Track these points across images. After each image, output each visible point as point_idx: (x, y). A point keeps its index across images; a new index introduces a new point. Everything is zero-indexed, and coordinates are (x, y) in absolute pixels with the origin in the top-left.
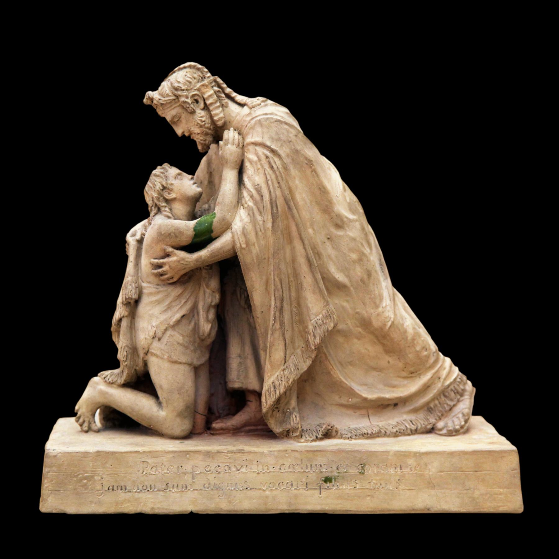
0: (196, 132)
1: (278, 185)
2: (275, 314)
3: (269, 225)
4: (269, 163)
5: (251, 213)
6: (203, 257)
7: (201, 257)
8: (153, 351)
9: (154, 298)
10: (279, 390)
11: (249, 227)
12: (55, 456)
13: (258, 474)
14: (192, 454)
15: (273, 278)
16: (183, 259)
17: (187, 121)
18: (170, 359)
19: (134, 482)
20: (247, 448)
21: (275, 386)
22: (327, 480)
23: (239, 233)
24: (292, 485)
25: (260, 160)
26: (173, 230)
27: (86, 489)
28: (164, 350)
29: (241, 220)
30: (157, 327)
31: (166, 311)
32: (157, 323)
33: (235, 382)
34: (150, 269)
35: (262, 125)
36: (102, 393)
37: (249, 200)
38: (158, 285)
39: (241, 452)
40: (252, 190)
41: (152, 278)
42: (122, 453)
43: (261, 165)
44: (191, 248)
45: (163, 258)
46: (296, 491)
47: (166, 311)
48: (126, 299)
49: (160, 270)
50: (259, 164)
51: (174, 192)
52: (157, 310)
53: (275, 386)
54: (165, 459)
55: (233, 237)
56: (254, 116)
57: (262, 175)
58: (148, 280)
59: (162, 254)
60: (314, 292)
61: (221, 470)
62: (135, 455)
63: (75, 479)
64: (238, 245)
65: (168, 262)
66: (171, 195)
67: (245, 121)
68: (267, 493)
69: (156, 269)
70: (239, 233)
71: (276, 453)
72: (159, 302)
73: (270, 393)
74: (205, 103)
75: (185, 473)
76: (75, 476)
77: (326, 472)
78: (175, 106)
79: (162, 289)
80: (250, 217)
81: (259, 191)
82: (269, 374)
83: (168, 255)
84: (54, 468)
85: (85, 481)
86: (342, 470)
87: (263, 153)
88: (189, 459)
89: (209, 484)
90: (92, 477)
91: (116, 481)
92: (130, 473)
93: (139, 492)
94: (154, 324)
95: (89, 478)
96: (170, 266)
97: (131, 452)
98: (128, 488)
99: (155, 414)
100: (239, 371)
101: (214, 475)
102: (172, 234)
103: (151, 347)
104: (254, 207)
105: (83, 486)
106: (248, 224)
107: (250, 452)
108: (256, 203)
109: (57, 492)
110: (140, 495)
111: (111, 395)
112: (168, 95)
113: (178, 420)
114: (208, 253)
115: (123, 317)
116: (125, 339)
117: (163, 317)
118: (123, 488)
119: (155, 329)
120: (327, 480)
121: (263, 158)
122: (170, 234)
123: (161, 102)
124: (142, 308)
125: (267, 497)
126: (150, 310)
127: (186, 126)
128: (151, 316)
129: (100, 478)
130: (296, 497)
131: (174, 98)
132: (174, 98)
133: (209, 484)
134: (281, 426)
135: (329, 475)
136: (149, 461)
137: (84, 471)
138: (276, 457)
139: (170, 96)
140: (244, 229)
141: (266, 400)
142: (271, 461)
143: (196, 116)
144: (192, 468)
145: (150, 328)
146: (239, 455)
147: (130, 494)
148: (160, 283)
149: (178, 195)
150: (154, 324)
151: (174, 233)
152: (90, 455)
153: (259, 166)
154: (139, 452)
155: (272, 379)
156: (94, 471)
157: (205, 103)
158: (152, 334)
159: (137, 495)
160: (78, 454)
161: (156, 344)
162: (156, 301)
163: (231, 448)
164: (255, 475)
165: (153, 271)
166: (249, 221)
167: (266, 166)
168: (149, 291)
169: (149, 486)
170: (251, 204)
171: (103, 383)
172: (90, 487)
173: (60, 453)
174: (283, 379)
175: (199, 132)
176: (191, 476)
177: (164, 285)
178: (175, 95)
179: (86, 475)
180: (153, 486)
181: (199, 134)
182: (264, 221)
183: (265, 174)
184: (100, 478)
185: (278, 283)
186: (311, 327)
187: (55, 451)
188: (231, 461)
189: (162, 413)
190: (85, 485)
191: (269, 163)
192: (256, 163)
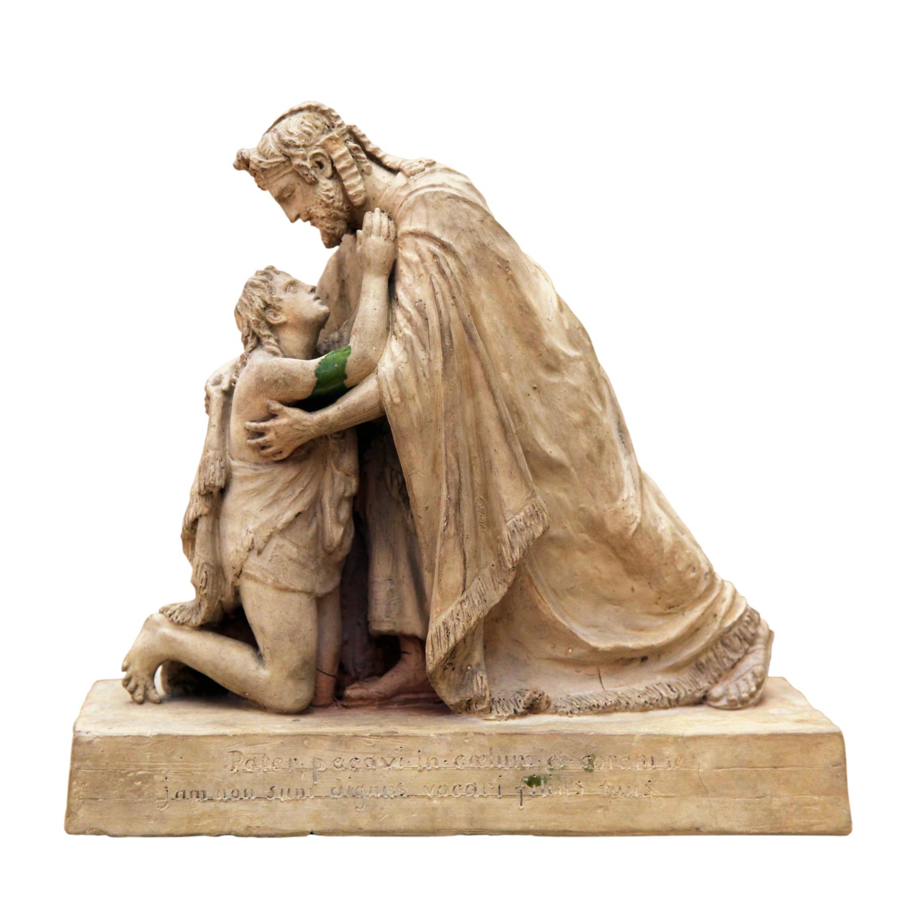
0: (319, 215)
1: (452, 301)
2: (447, 510)
3: (438, 366)
4: (439, 265)
5: (408, 347)
6: (331, 419)
7: (327, 418)
8: (248, 571)
9: (250, 486)
10: (455, 634)
11: (406, 370)
12: (90, 743)
13: (420, 771)
14: (312, 739)
15: (444, 452)
16: (298, 422)
17: (305, 197)
18: (277, 584)
19: (218, 784)
20: (402, 730)
21: (447, 629)
22: (533, 781)
23: (389, 379)
24: (475, 789)
25: (423, 261)
26: (281, 374)
27: (140, 796)
28: (266, 570)
29: (393, 359)
30: (256, 532)
31: (269, 505)
32: (256, 526)
33: (383, 621)
34: (244, 439)
35: (426, 204)
36: (166, 640)
37: (405, 326)
38: (257, 464)
39: (392, 735)
40: (409, 309)
41: (247, 453)
42: (198, 737)
43: (426, 268)
44: (311, 404)
45: (265, 420)
46: (482, 800)
47: (269, 505)
48: (205, 486)
49: (260, 440)
50: (421, 266)
51: (283, 312)
52: (255, 505)
53: (447, 629)
54: (268, 747)
55: (379, 386)
56: (414, 189)
57: (426, 285)
58: (242, 456)
59: (264, 413)
60: (511, 476)
61: (359, 765)
62: (219, 740)
63: (122, 780)
64: (388, 399)
65: (273, 427)
66: (278, 318)
67: (398, 196)
68: (435, 802)
69: (253, 438)
70: (389, 379)
71: (449, 738)
72: (258, 492)
73: (439, 640)
74: (334, 168)
75: (301, 771)
76: (123, 776)
77: (531, 768)
78: (285, 172)
79: (264, 471)
80: (408, 353)
81: (421, 310)
82: (438, 610)
83: (273, 416)
84: (88, 763)
85: (139, 783)
86: (557, 765)
87: (429, 250)
88: (307, 747)
89: (341, 788)
90: (151, 776)
91: (189, 783)
92: (212, 771)
93: (226, 802)
94: (251, 528)
95: (145, 779)
96: (276, 433)
97: (213, 736)
98: (208, 794)
99: (253, 674)
100: (389, 604)
101: (348, 774)
102: (280, 381)
103: (245, 566)
104: (414, 338)
105: (134, 791)
106: (403, 365)
107: (407, 736)
108: (416, 331)
109: (93, 802)
110: (228, 806)
111: (181, 643)
112: (273, 155)
113: (290, 683)
114: (339, 412)
115: (201, 516)
116: (203, 551)
117: (265, 517)
118: (200, 795)
119: (252, 535)
120: (533, 781)
121: (428, 257)
122: (276, 381)
123: (262, 165)
124: (232, 502)
125: (434, 809)
126: (244, 504)
127: (304, 205)
128: (246, 515)
129: (162, 778)
130: (482, 808)
131: (283, 159)
132: (283, 159)
133: (341, 788)
134: (458, 694)
135: (536, 773)
136: (243, 750)
137: (136, 766)
138: (449, 744)
139: (277, 156)
140: (397, 372)
141: (433, 651)
142: (442, 750)
143: (319, 189)
144: (313, 762)
145: (244, 534)
146: (388, 741)
147: (212, 804)
148: (260, 460)
149: (290, 317)
150: (251, 528)
151: (284, 379)
152: (147, 741)
153: (422, 271)
154: (226, 735)
155: (443, 617)
156: (154, 767)
157: (334, 168)
158: (247, 543)
159: (223, 806)
160: (127, 740)
161: (253, 560)
162: (254, 490)
163: (375, 729)
164: (415, 773)
165: (249, 441)
166: (406, 360)
167: (434, 271)
168: (242, 475)
169: (242, 792)
170: (408, 332)
171: (168, 624)
172: (146, 793)
173: (98, 737)
174: (460, 617)
175: (324, 215)
176: (310, 774)
177: (267, 464)
178: (285, 155)
179: (140, 773)
180: (248, 791)
181: (323, 217)
182: (430, 360)
183: (431, 283)
184: (162, 778)
185: (453, 461)
186: (506, 533)
187: (89, 735)
188: (376, 750)
189: (265, 673)
190: (139, 789)
191: (439, 265)
192: (417, 265)
